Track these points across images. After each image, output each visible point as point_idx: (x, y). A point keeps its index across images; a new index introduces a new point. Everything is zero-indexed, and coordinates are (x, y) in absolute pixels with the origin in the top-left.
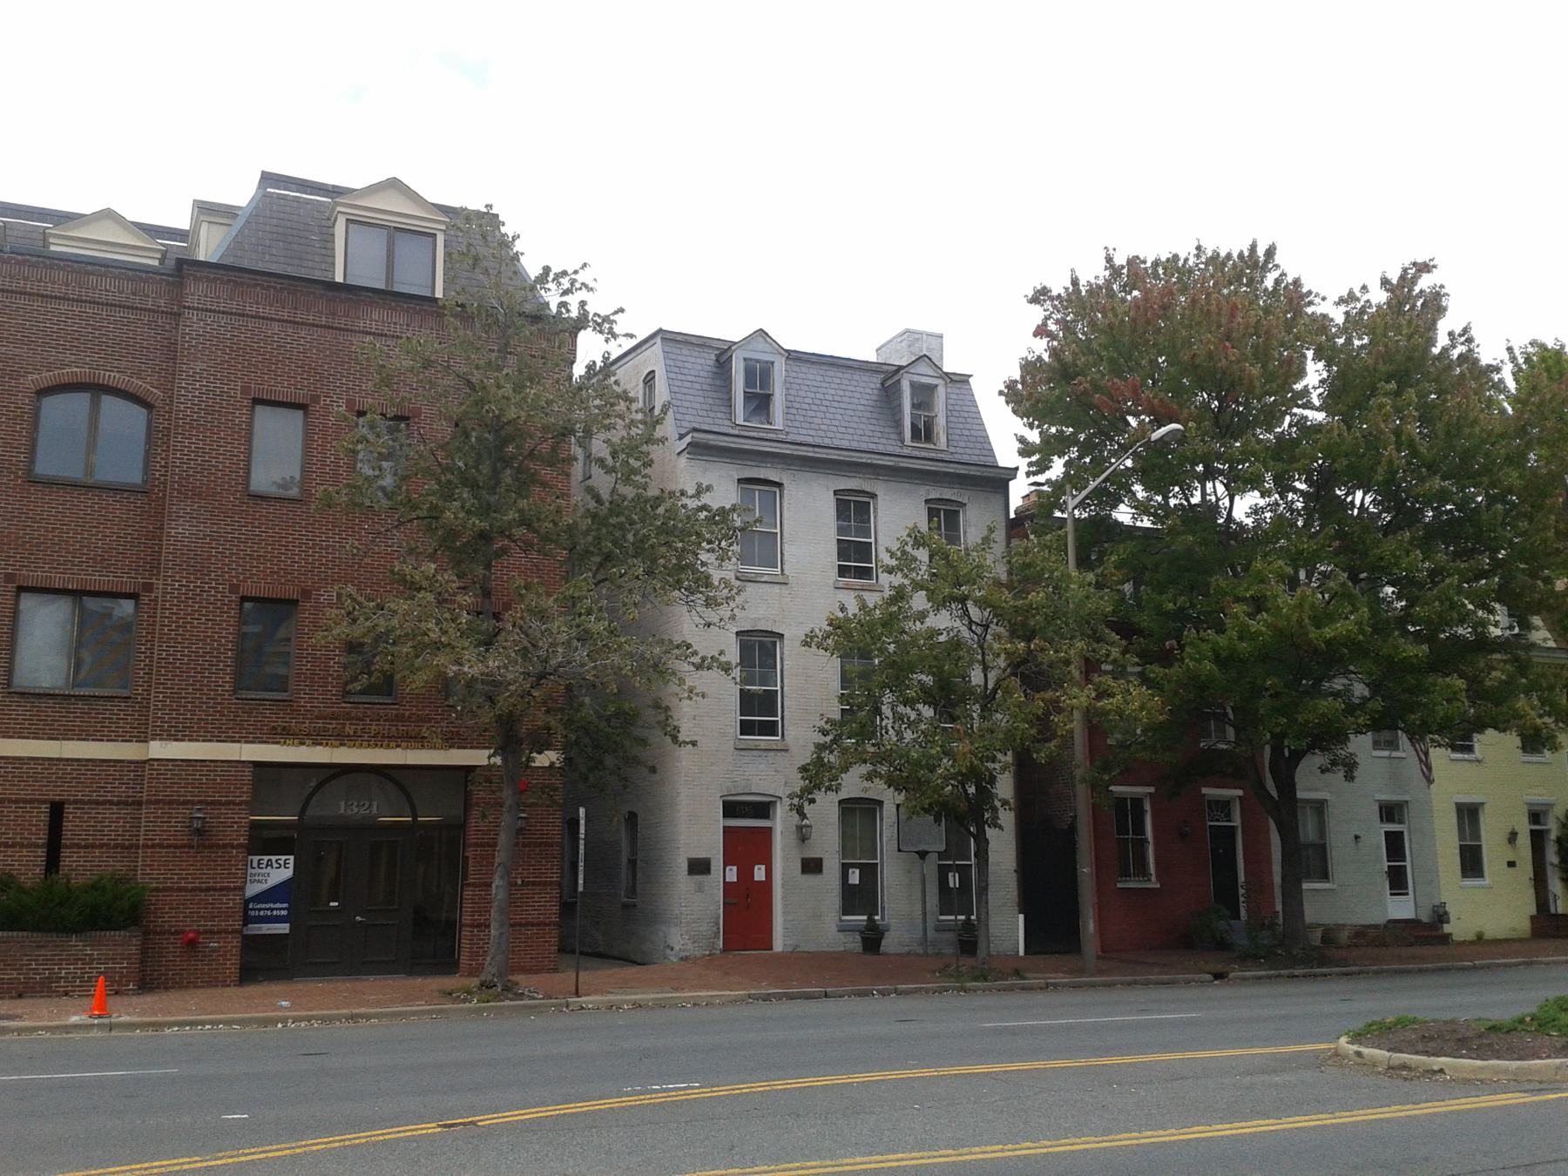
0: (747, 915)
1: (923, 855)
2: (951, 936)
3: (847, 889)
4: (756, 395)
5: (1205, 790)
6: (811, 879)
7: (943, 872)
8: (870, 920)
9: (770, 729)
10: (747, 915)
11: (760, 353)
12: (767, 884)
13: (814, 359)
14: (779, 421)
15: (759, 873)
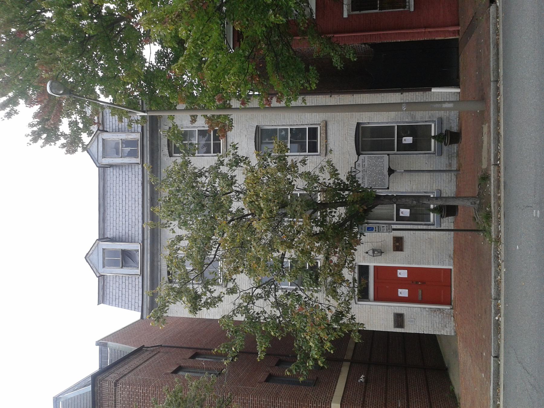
0: (429, 287)
1: (391, 171)
2: (445, 148)
3: (413, 217)
4: (123, 259)
5: (345, 15)
6: (407, 244)
7: (403, 148)
8: (434, 211)
9: (313, 132)
10: (429, 287)
11: (98, 258)
12: (410, 270)
13: (102, 210)
14: (136, 247)
15: (403, 274)
